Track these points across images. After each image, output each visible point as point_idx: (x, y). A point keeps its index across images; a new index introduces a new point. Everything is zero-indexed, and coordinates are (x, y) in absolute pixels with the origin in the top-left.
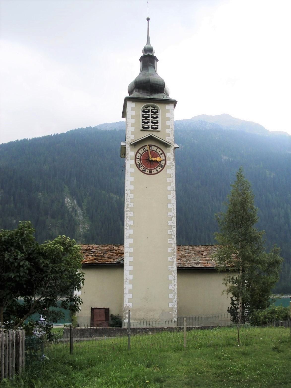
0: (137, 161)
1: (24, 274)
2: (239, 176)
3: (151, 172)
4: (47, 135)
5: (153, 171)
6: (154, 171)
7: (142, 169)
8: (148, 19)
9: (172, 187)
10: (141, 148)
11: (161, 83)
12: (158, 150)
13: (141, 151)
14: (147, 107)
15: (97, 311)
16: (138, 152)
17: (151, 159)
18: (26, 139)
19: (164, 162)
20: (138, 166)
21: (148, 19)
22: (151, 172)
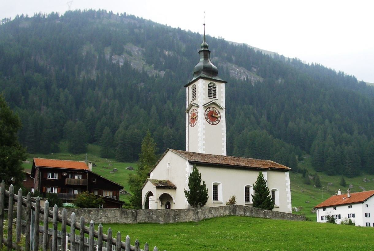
0: (206, 116)
1: (103, 195)
2: (271, 54)
3: (213, 123)
4: (142, 18)
5: (214, 122)
6: (215, 123)
7: (208, 120)
8: (204, 25)
9: (224, 129)
10: (207, 109)
11: (124, 247)
12: (217, 111)
13: (208, 110)
14: (210, 83)
15: (182, 210)
16: (206, 110)
17: (214, 115)
18: (78, 10)
19: (220, 118)
20: (206, 119)
21: (204, 25)
22: (213, 123)
